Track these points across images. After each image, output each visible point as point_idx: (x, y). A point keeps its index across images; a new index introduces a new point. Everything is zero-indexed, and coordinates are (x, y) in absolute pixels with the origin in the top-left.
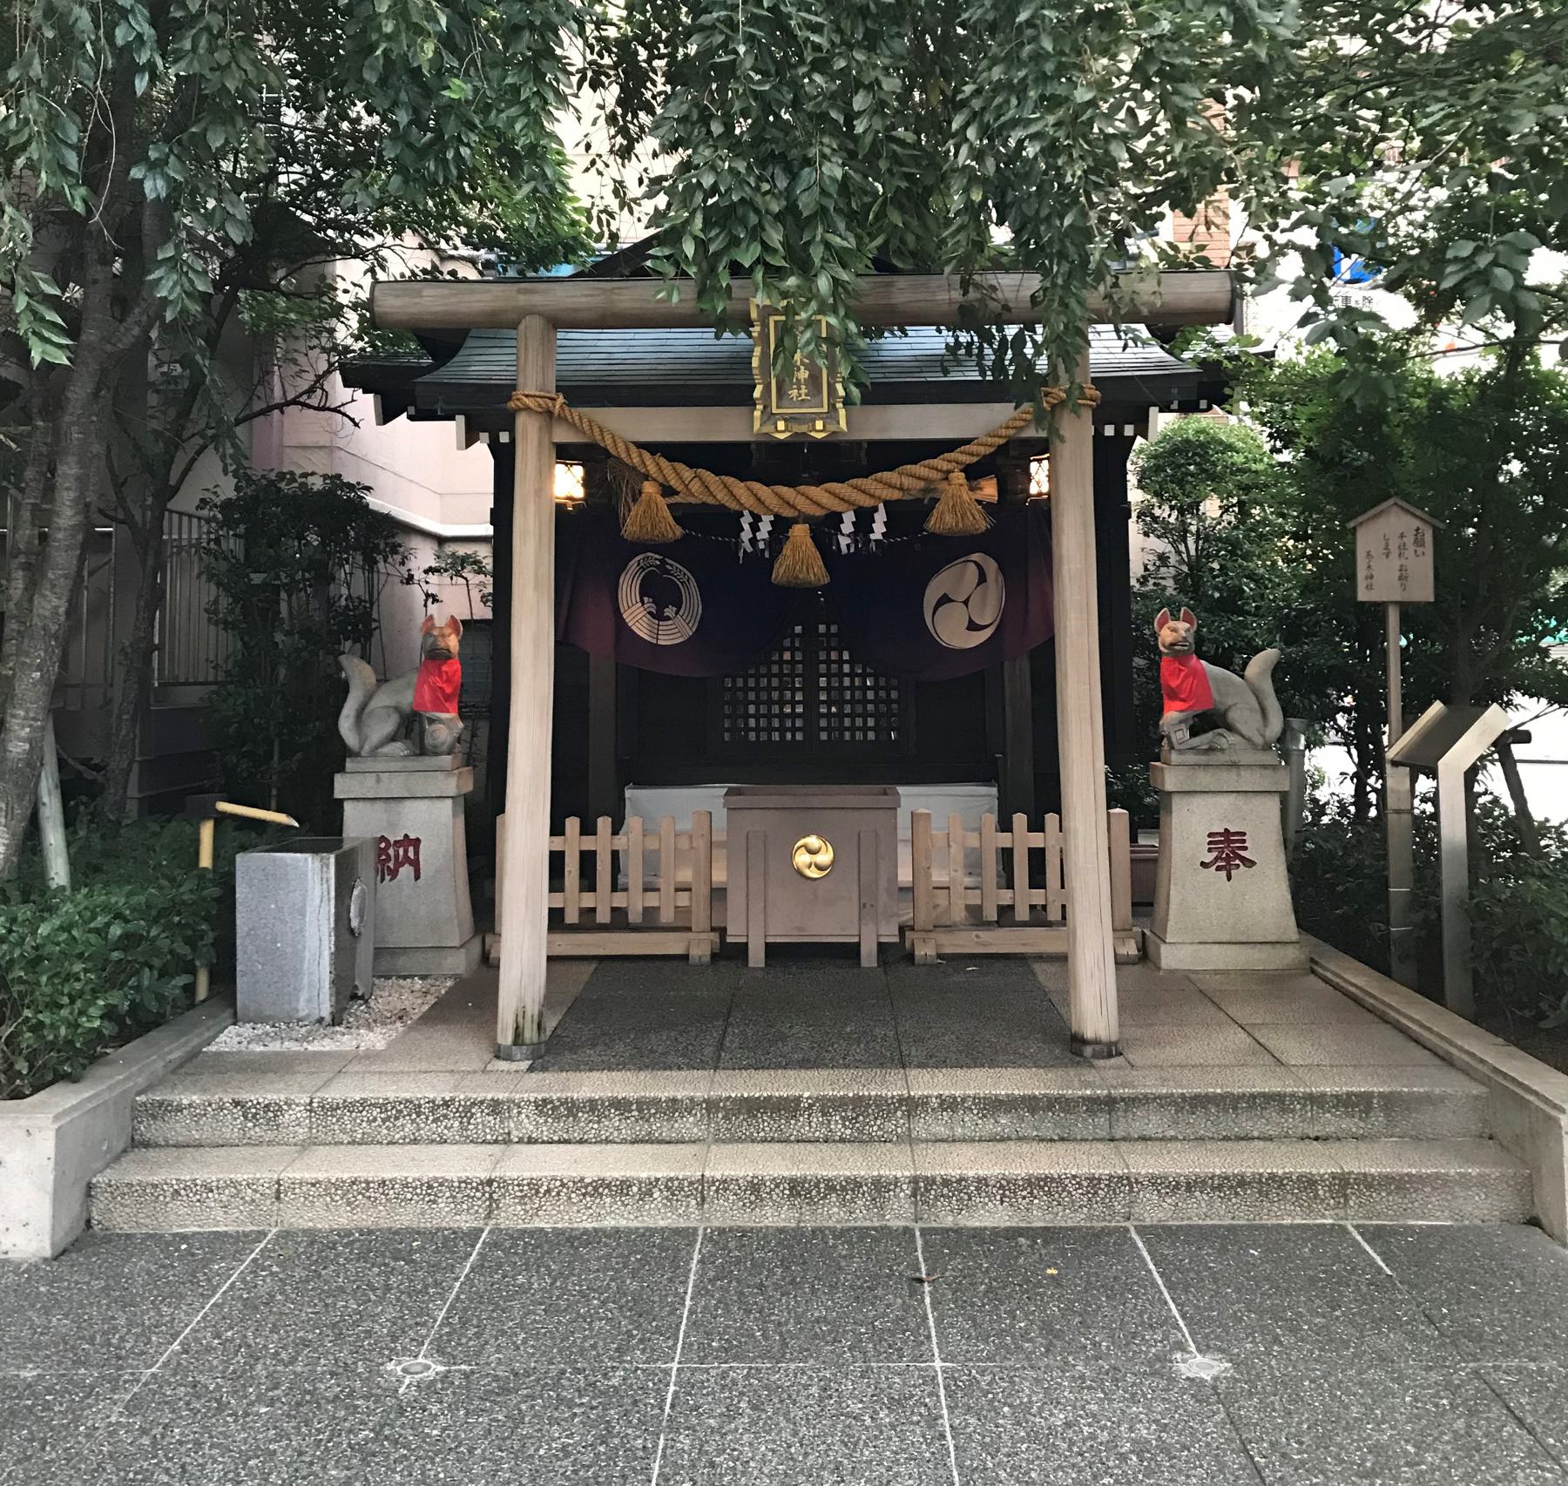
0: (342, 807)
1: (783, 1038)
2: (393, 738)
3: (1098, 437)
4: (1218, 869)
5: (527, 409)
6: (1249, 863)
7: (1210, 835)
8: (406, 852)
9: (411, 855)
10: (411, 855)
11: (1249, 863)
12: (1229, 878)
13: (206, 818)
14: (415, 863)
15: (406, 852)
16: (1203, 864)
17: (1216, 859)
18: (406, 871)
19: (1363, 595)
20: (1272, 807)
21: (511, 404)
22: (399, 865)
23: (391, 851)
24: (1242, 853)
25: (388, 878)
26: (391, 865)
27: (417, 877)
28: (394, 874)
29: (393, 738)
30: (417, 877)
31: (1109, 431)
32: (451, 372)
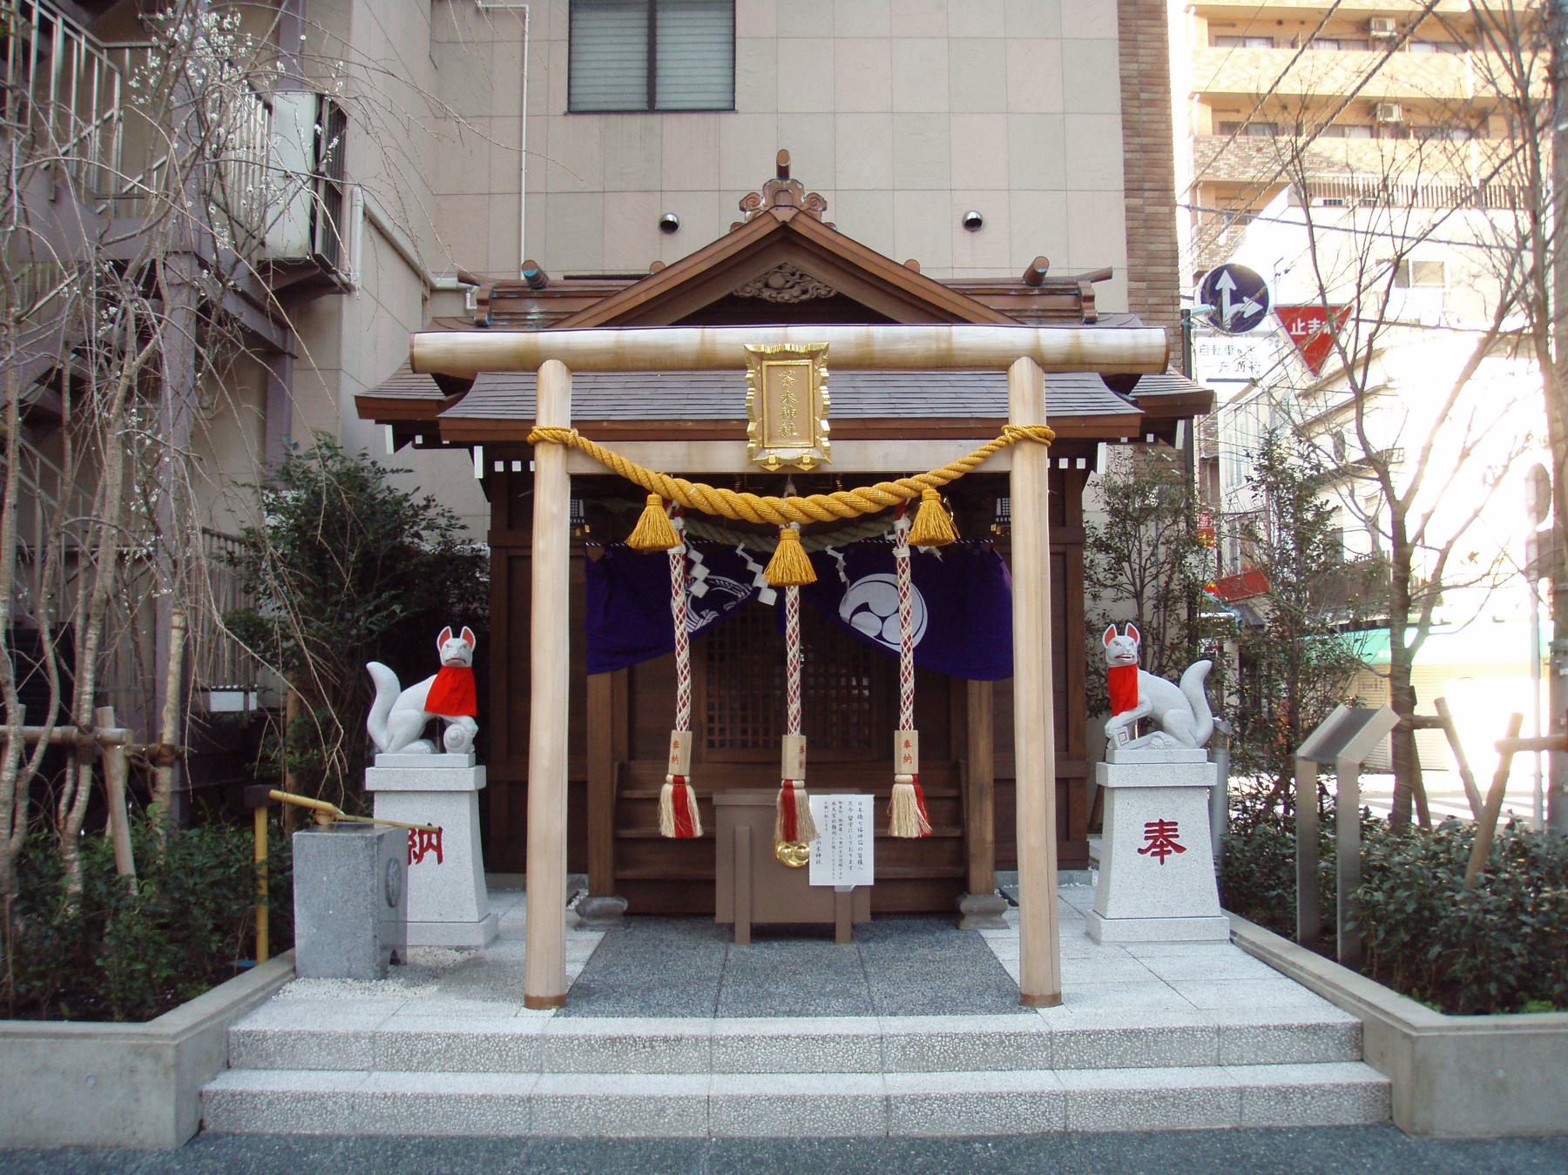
0: (372, 801)
1: (770, 995)
2: (1498, 92)
3: (1054, 471)
4: (1154, 854)
5: (543, 440)
6: (1180, 849)
7: (1148, 825)
8: (430, 839)
9: (434, 841)
10: (434, 841)
11: (1180, 849)
12: (1162, 861)
13: (260, 805)
14: (438, 848)
15: (430, 839)
16: (1140, 851)
17: (1154, 845)
18: (430, 855)
19: (871, 883)
20: (1201, 803)
21: (530, 437)
22: (423, 850)
23: (417, 838)
24: (1173, 840)
25: (414, 861)
26: (417, 850)
27: (440, 860)
28: (419, 857)
29: (1498, 92)
30: (440, 860)
31: (1063, 464)
32: (464, 409)
